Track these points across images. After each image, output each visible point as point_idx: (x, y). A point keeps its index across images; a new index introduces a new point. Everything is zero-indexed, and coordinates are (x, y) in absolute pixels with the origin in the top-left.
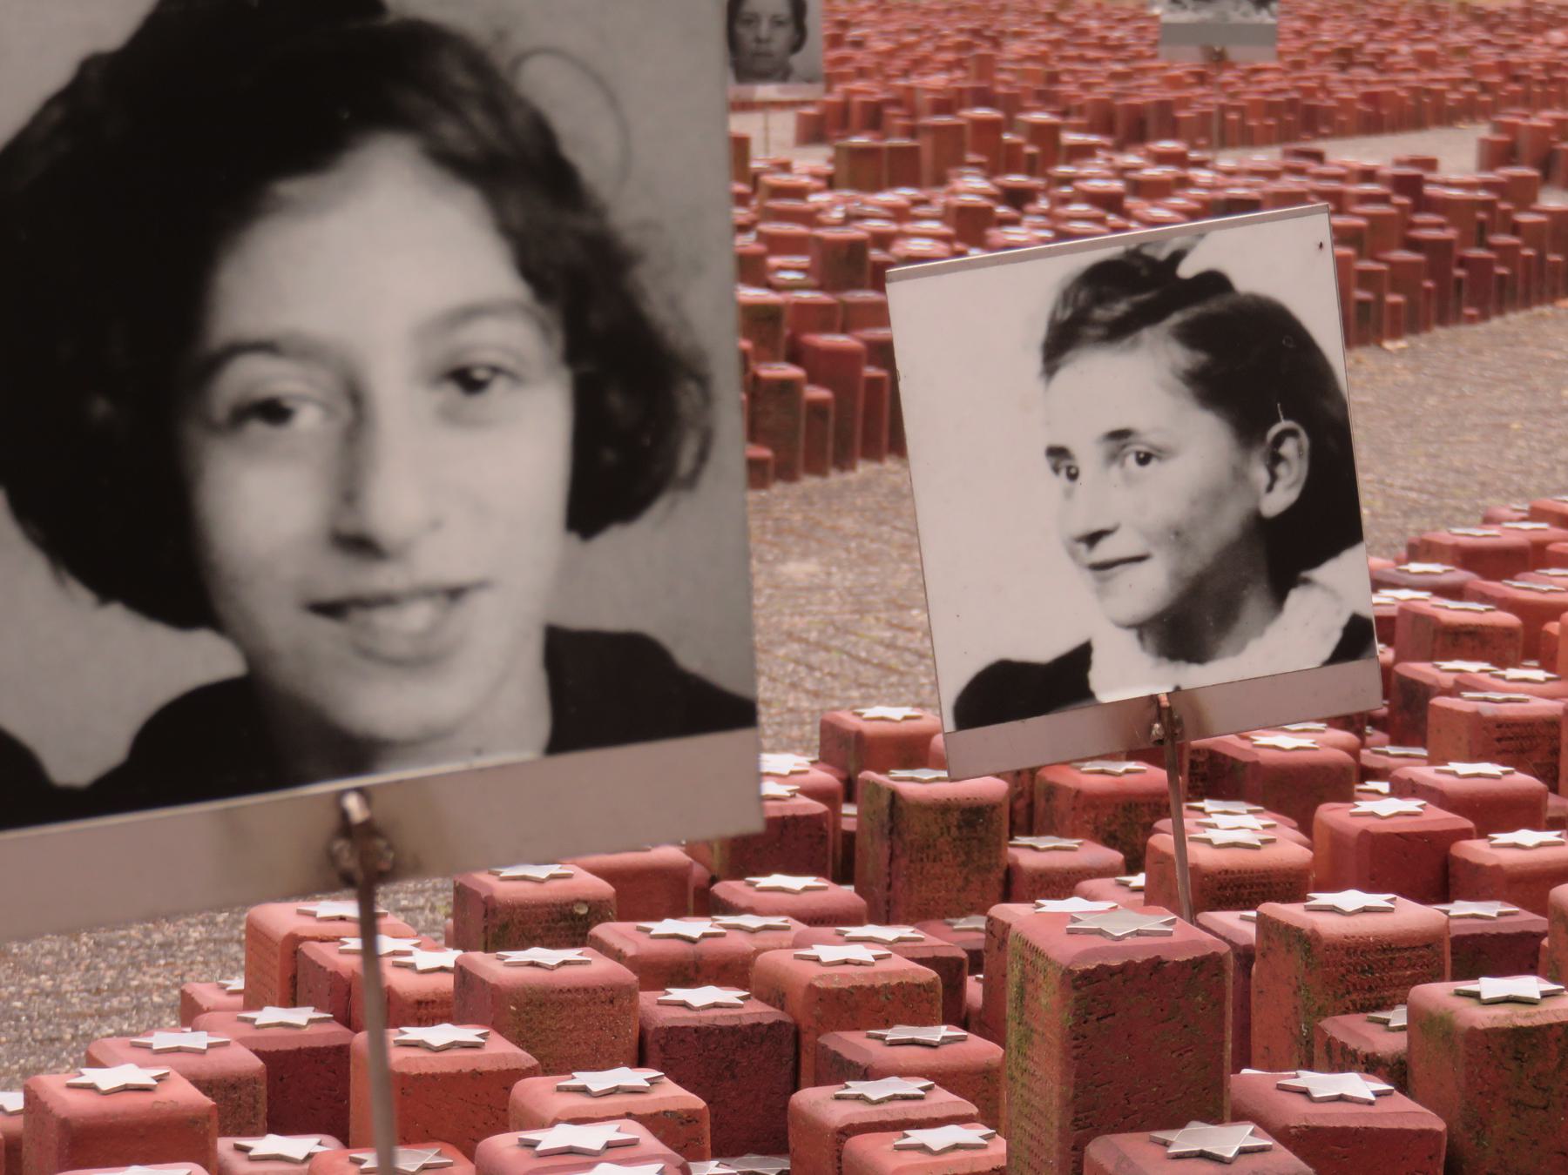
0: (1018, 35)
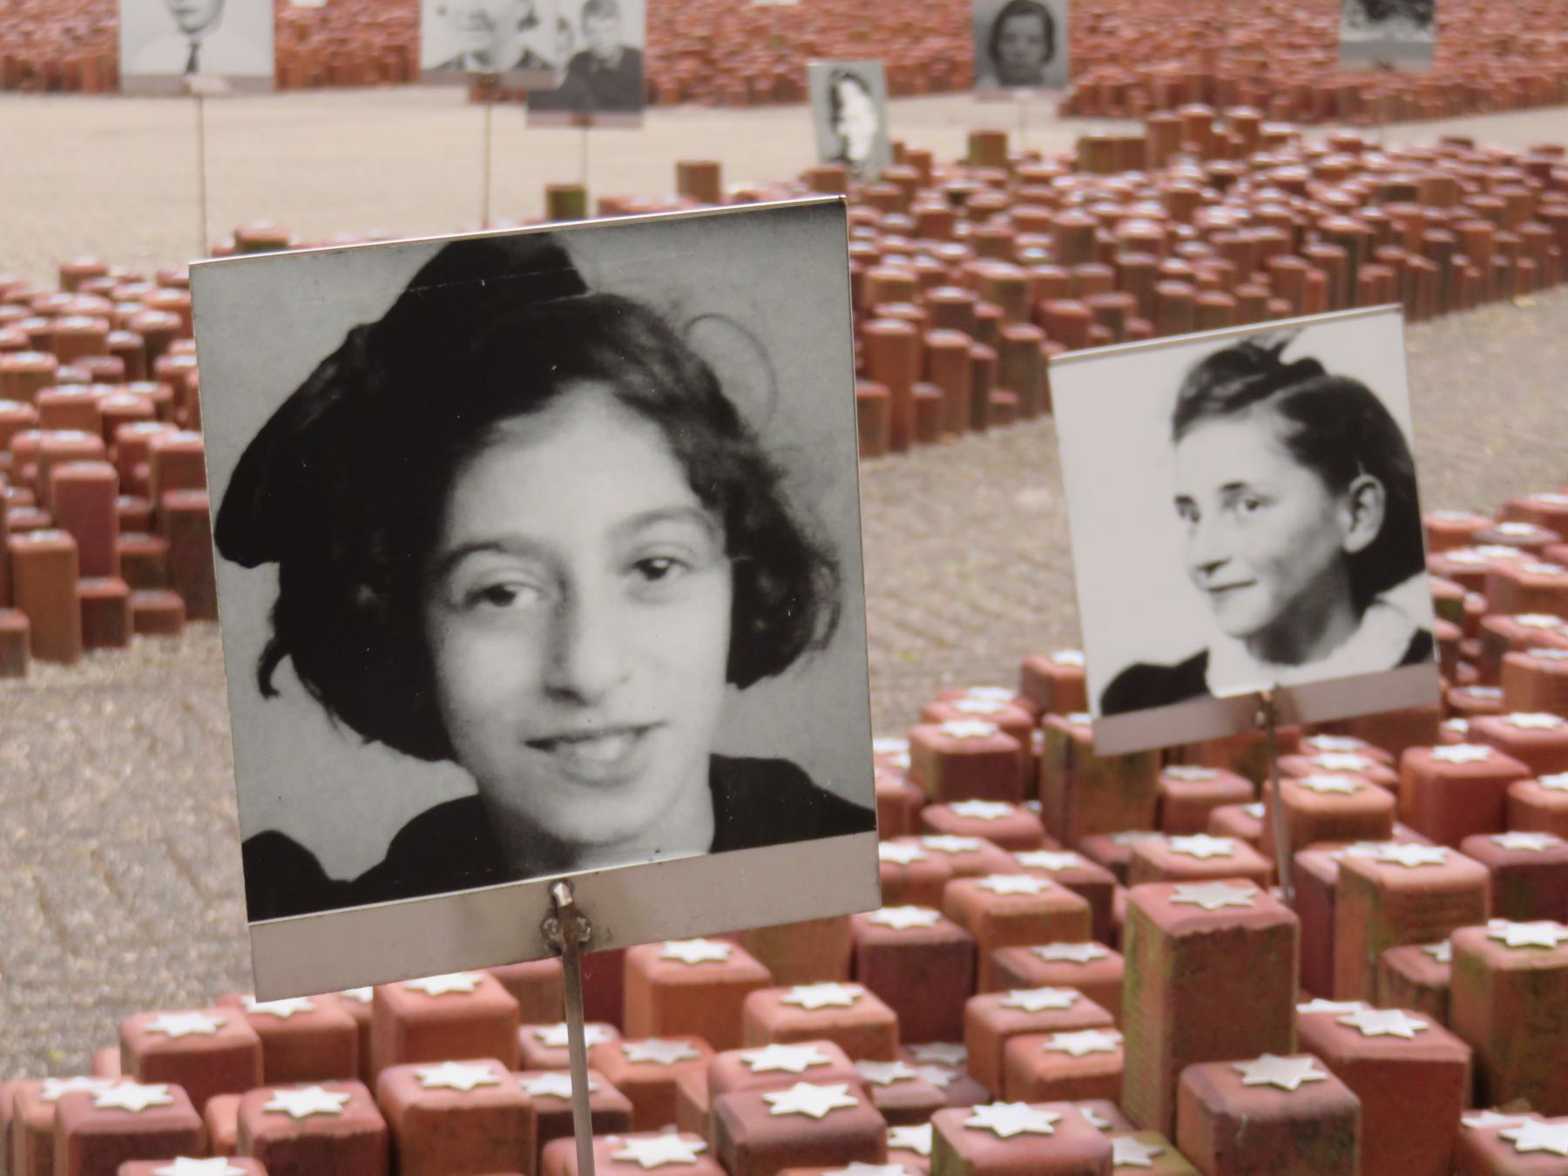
0: (1241, 25)
